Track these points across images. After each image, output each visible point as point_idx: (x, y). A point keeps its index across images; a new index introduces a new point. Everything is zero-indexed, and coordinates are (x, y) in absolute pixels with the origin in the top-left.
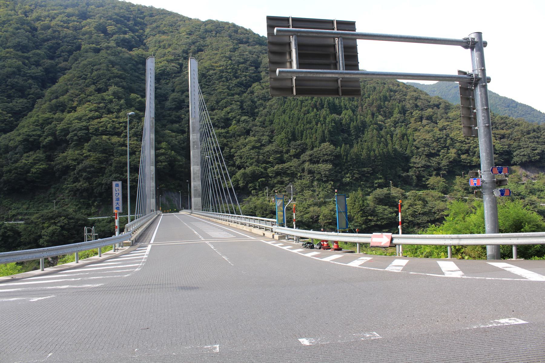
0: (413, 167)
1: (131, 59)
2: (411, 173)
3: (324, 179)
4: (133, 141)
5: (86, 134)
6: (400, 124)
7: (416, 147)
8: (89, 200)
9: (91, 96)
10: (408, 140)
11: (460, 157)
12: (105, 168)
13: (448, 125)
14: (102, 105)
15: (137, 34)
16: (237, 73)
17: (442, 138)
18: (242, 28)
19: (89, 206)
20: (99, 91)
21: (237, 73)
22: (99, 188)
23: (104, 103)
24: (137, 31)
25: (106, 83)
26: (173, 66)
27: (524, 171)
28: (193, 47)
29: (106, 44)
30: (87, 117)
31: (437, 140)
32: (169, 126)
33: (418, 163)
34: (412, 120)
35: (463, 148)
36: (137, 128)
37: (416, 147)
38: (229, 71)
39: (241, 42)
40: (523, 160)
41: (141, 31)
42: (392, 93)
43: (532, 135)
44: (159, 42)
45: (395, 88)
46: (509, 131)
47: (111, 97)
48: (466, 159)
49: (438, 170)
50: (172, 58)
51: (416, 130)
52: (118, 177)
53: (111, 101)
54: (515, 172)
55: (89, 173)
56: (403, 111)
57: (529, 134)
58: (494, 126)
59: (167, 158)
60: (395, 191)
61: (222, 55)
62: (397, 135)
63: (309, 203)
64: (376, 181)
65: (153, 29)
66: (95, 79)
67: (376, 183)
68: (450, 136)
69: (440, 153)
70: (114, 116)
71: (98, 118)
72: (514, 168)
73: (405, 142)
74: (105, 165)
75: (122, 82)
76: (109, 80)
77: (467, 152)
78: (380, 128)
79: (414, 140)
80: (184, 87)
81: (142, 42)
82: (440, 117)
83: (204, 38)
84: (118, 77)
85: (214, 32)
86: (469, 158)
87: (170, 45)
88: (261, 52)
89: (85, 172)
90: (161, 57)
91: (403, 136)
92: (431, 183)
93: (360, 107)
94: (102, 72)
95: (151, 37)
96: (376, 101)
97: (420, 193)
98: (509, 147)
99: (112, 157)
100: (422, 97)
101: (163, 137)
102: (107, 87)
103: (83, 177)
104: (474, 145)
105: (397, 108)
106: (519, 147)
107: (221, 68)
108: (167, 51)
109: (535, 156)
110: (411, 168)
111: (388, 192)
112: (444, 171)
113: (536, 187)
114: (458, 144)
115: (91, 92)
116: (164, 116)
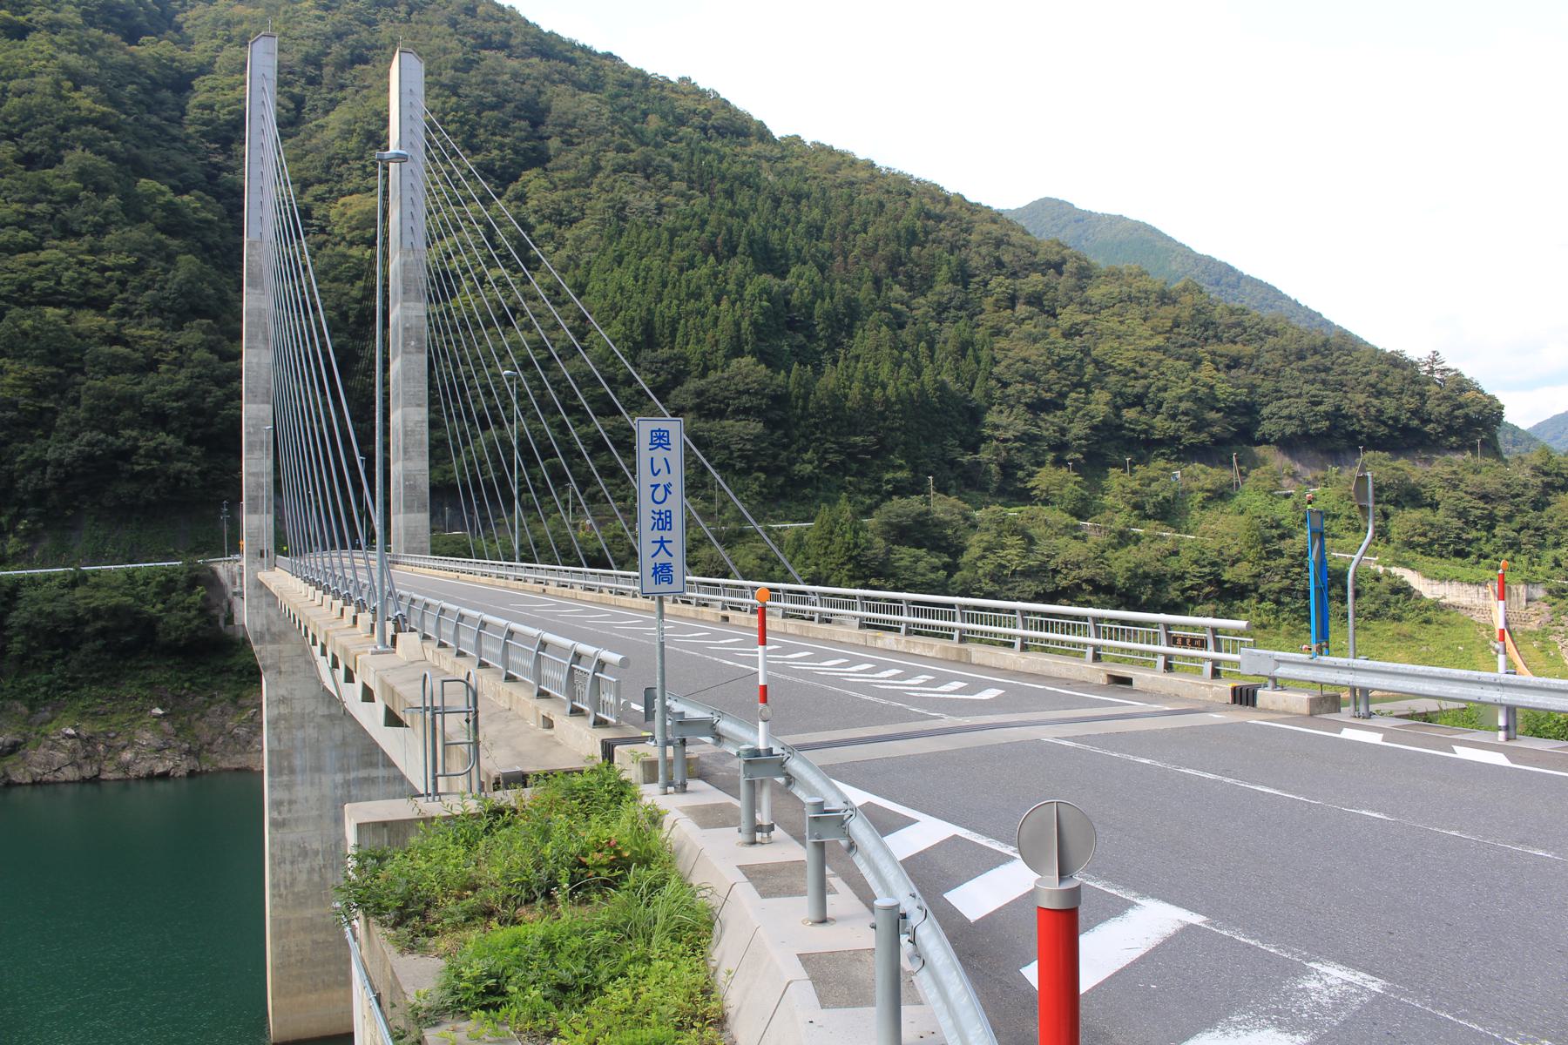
0: (990, 437)
1: (133, 68)
2: (984, 455)
3: (738, 466)
4: (151, 328)
10: (978, 362)
11: (1119, 416)
12: (55, 412)
14: (39, 208)
16: (476, 136)
20: (30, 161)
21: (476, 136)
22: (35, 476)
23: (50, 202)
25: (54, 138)
27: (1287, 461)
29: (49, 13)
31: (1059, 364)
33: (1006, 428)
34: (988, 303)
35: (1129, 390)
36: (162, 288)
37: (999, 380)
39: (488, 45)
40: (1288, 431)
42: (931, 223)
43: (1310, 361)
44: (228, 23)
45: (938, 208)
46: (1250, 350)
47: (72, 184)
48: (1137, 422)
49: (1061, 447)
51: (997, 332)
53: (72, 199)
56: (963, 276)
57: (1302, 358)
58: (1210, 333)
60: (943, 507)
62: (945, 342)
63: (697, 536)
64: (888, 476)
66: (15, 124)
67: (888, 482)
68: (1094, 353)
69: (1067, 402)
70: (85, 247)
71: (25, 248)
72: (1260, 451)
73: (968, 365)
75: (107, 140)
77: (1138, 401)
78: (898, 323)
79: (995, 362)
80: (308, 169)
81: (170, 21)
83: (371, 23)
84: (95, 122)
86: (1143, 418)
88: (547, 77)
91: (964, 347)
92: (1043, 487)
93: (840, 258)
94: (36, 100)
96: (886, 244)
97: (1012, 512)
98: (1250, 393)
99: (79, 378)
100: (1015, 237)
102: (58, 150)
104: (1161, 383)
105: (945, 268)
106: (1278, 394)
109: (1316, 422)
110: (984, 439)
111: (924, 507)
114: (1113, 378)
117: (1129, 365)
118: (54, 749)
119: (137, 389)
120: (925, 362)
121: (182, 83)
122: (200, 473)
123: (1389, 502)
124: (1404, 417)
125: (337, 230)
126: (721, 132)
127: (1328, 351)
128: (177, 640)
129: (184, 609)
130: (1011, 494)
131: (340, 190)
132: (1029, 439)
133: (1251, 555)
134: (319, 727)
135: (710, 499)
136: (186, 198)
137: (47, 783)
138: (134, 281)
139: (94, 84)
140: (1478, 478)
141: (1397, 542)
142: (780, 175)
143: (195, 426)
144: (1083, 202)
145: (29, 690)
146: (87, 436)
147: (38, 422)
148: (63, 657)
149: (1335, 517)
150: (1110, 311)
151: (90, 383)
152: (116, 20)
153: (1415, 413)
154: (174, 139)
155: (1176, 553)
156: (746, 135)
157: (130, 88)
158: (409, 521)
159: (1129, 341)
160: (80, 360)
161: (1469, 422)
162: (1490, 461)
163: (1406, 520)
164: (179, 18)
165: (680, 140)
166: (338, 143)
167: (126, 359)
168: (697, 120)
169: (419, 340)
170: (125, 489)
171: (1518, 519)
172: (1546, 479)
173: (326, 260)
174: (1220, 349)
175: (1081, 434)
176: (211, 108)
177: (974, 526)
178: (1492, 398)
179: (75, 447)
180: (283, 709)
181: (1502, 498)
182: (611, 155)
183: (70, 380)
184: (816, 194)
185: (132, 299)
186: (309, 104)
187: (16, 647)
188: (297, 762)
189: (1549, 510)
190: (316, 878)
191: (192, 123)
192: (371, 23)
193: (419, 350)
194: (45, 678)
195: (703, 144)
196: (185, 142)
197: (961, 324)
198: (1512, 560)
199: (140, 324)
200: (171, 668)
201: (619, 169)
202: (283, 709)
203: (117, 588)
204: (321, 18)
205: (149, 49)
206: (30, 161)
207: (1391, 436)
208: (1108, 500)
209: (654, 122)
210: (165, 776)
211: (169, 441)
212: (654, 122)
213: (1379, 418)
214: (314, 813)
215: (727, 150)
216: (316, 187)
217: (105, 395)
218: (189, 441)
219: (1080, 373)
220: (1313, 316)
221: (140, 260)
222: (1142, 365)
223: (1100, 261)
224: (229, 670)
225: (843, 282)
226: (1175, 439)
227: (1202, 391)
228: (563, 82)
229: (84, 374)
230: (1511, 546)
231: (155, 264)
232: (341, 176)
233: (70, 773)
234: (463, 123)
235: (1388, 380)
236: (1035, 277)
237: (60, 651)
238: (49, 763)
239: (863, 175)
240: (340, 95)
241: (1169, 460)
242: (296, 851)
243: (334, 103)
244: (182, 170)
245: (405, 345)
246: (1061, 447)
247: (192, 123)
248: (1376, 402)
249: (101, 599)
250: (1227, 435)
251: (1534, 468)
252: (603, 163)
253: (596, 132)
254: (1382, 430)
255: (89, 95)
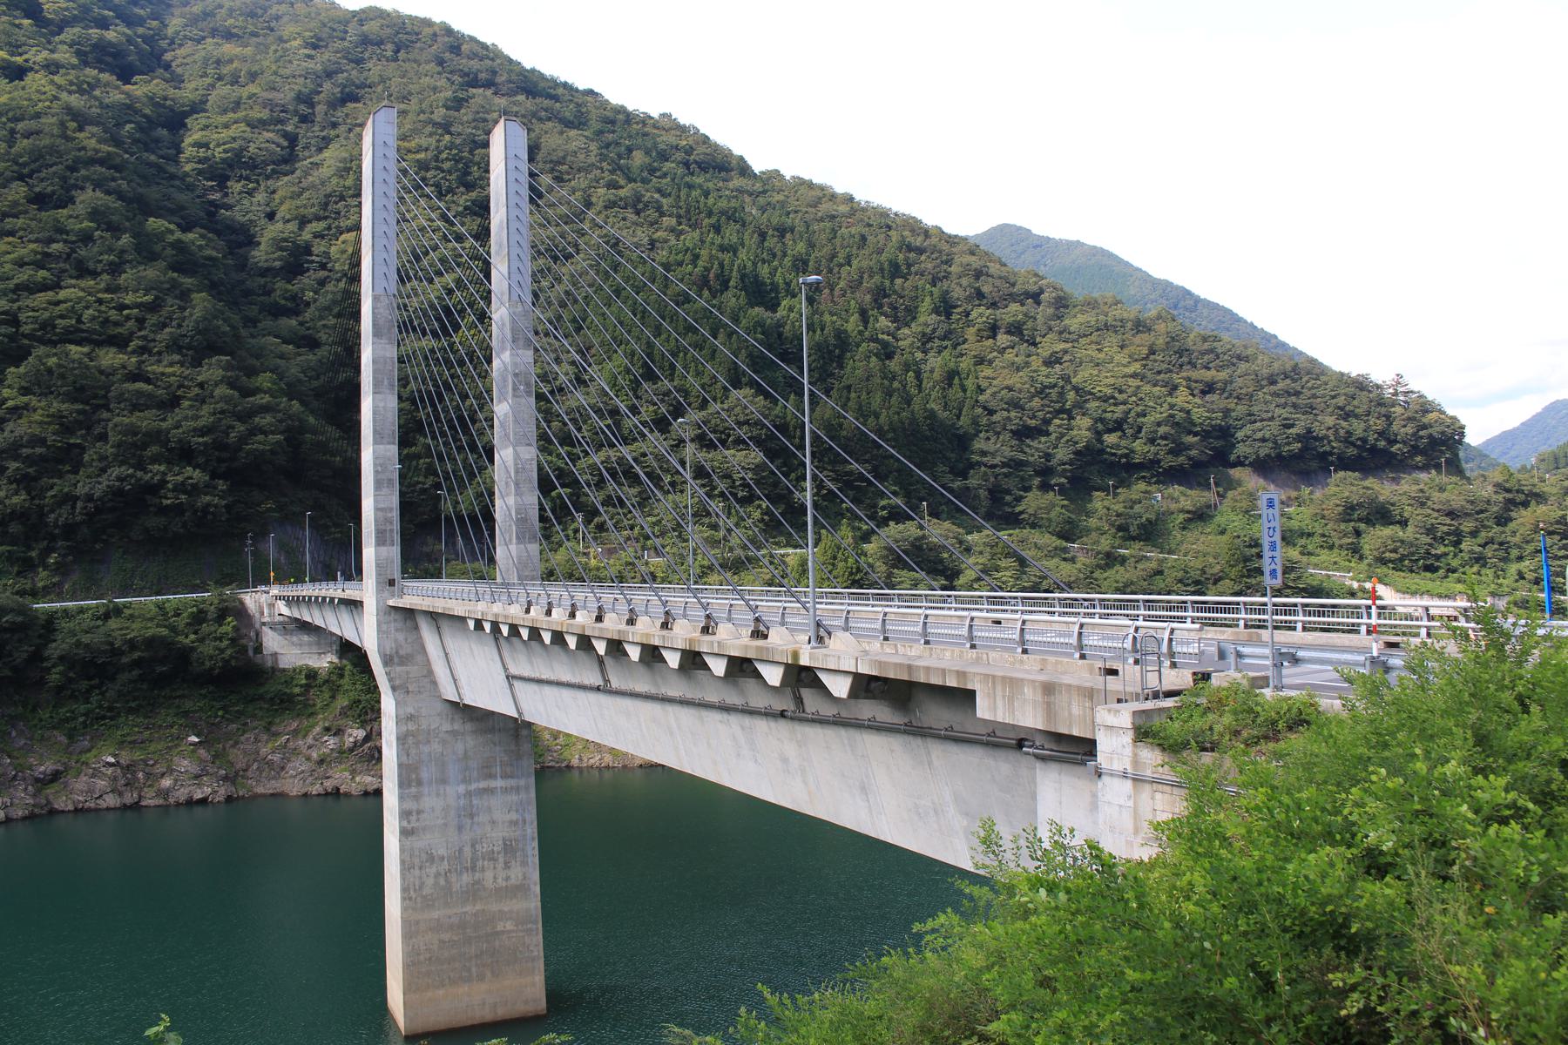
0: (979, 464)
1: (129, 107)
2: (973, 482)
3: (740, 494)
4: (171, 365)
5: (12, 338)
6: (937, 342)
7: (985, 408)
8: (30, 548)
9: (16, 216)
10: (964, 391)
11: (1101, 442)
12: (82, 449)
13: (1065, 352)
14: (56, 247)
15: (140, 30)
16: (470, 174)
17: (1055, 386)
18: (473, 39)
19: (27, 567)
20: (41, 200)
21: (470, 174)
22: (64, 511)
23: (65, 241)
24: (141, 22)
25: (64, 179)
26: (265, 142)
27: (1261, 481)
28: (327, 86)
29: (45, 54)
30: (11, 284)
31: (1042, 392)
32: (267, 323)
33: (993, 455)
34: (970, 333)
35: (1109, 415)
36: (180, 326)
37: (985, 408)
38: (447, 165)
39: (474, 82)
40: (1262, 453)
41: (155, 23)
42: (912, 255)
43: (1281, 385)
44: (218, 62)
45: (918, 241)
46: (1223, 375)
47: (86, 224)
48: (1118, 446)
49: (1045, 472)
50: (265, 114)
51: (980, 361)
52: (131, 476)
53: (86, 238)
54: (1239, 483)
55: (29, 461)
56: (945, 307)
57: (1273, 383)
58: (1185, 359)
59: (280, 421)
60: (938, 531)
61: (422, 117)
62: (932, 371)
63: (706, 563)
64: (883, 503)
65: (194, 21)
66: (25, 165)
67: (883, 508)
68: (1074, 381)
69: (1051, 429)
70: (102, 285)
71: (44, 287)
72: (1236, 473)
73: (955, 393)
74: (82, 437)
75: (114, 179)
76: (72, 169)
77: (1118, 426)
78: (887, 353)
79: (980, 390)
80: (305, 206)
81: (159, 58)
82: (1042, 328)
83: (359, 62)
84: (101, 162)
85: (390, 47)
86: (1123, 443)
87: (253, 76)
88: (534, 115)
89: (16, 458)
90: (225, 111)
91: (951, 375)
92: (1031, 511)
93: (827, 291)
94: (46, 141)
95: (188, 48)
96: (871, 277)
97: (1004, 535)
98: (1225, 417)
99: (105, 415)
100: (994, 269)
101: (258, 357)
102: (68, 190)
103: (9, 473)
104: (1139, 409)
105: (928, 299)
106: (1251, 418)
107: (422, 156)
108: (245, 92)
109: (1289, 444)
110: (972, 465)
111: (920, 533)
112: (1061, 476)
113: (1295, 524)
114: (1093, 405)
115: (15, 203)
116: (247, 293)
117: (1109, 391)
118: (95, 778)
119: (164, 425)
120: (914, 391)
121: (175, 120)
122: (226, 506)
123: (1360, 520)
124: (1372, 438)
125: (337, 267)
126: (704, 167)
127: (1298, 377)
128: (211, 669)
129: (216, 639)
130: (1000, 517)
131: (338, 227)
132: (1016, 465)
133: (1233, 573)
134: (444, 742)
135: (715, 527)
136: (191, 236)
137: (89, 810)
138: (152, 319)
139: (97, 124)
140: (1445, 495)
141: (1370, 559)
142: (763, 210)
143: (220, 460)
144: (1039, 228)
145: (67, 720)
146: (116, 471)
147: (66, 458)
148: (99, 687)
149: (1310, 535)
150: (1088, 340)
151: (117, 419)
152: (109, 59)
153: (1381, 434)
154: (173, 177)
155: (1160, 573)
156: (728, 170)
157: (128, 127)
158: (375, 552)
159: (1106, 369)
160: (105, 397)
161: (1433, 442)
162: (1454, 479)
163: (1377, 537)
164: (168, 56)
165: (665, 175)
166: (334, 181)
167: (150, 396)
168: (679, 156)
169: (528, 385)
170: (153, 522)
171: (1483, 534)
172: (1509, 496)
173: (330, 296)
174: (1195, 374)
175: (1065, 459)
176: (206, 146)
177: (968, 550)
178: (1454, 418)
179: (105, 482)
180: (411, 727)
181: (1467, 514)
182: (602, 191)
183: (95, 417)
184: (800, 228)
185: (152, 336)
186: (302, 142)
187: (54, 677)
188: (424, 775)
189: (1512, 526)
190: (442, 882)
191: (188, 161)
192: (359, 62)
193: (528, 393)
194: (83, 708)
195: (687, 179)
196: (182, 179)
197: (946, 353)
198: (1479, 573)
199: (159, 361)
200: (205, 696)
201: (610, 205)
202: (411, 727)
203: (151, 619)
204: (310, 57)
205: (142, 88)
206: (41, 200)
207: (1359, 457)
208: (1093, 522)
209: (638, 158)
210: (203, 801)
211: (195, 475)
212: (638, 158)
213: (1347, 440)
214: (440, 822)
215: (710, 185)
216: (314, 224)
217: (133, 431)
218: (214, 476)
219: (1063, 401)
220: (1270, 338)
221: (157, 298)
222: (1121, 392)
223: (1077, 292)
224: (261, 698)
225: (832, 314)
226: (1155, 462)
227: (1180, 416)
228: (549, 119)
229: (109, 410)
230: (1477, 560)
231: (171, 303)
232: (338, 213)
233: (111, 801)
234: (457, 161)
235: (1355, 402)
236: (1014, 307)
237: (96, 681)
238: (90, 791)
239: (843, 209)
240: (333, 133)
241: (1150, 484)
242: (424, 856)
243: (326, 142)
244: (182, 208)
245: (515, 389)
246: (1045, 472)
247: (188, 161)
248: (1344, 424)
249: (136, 630)
250: (1204, 458)
251: (1497, 485)
252: (594, 200)
253: (586, 169)
254: (1352, 451)
255: (93, 135)
